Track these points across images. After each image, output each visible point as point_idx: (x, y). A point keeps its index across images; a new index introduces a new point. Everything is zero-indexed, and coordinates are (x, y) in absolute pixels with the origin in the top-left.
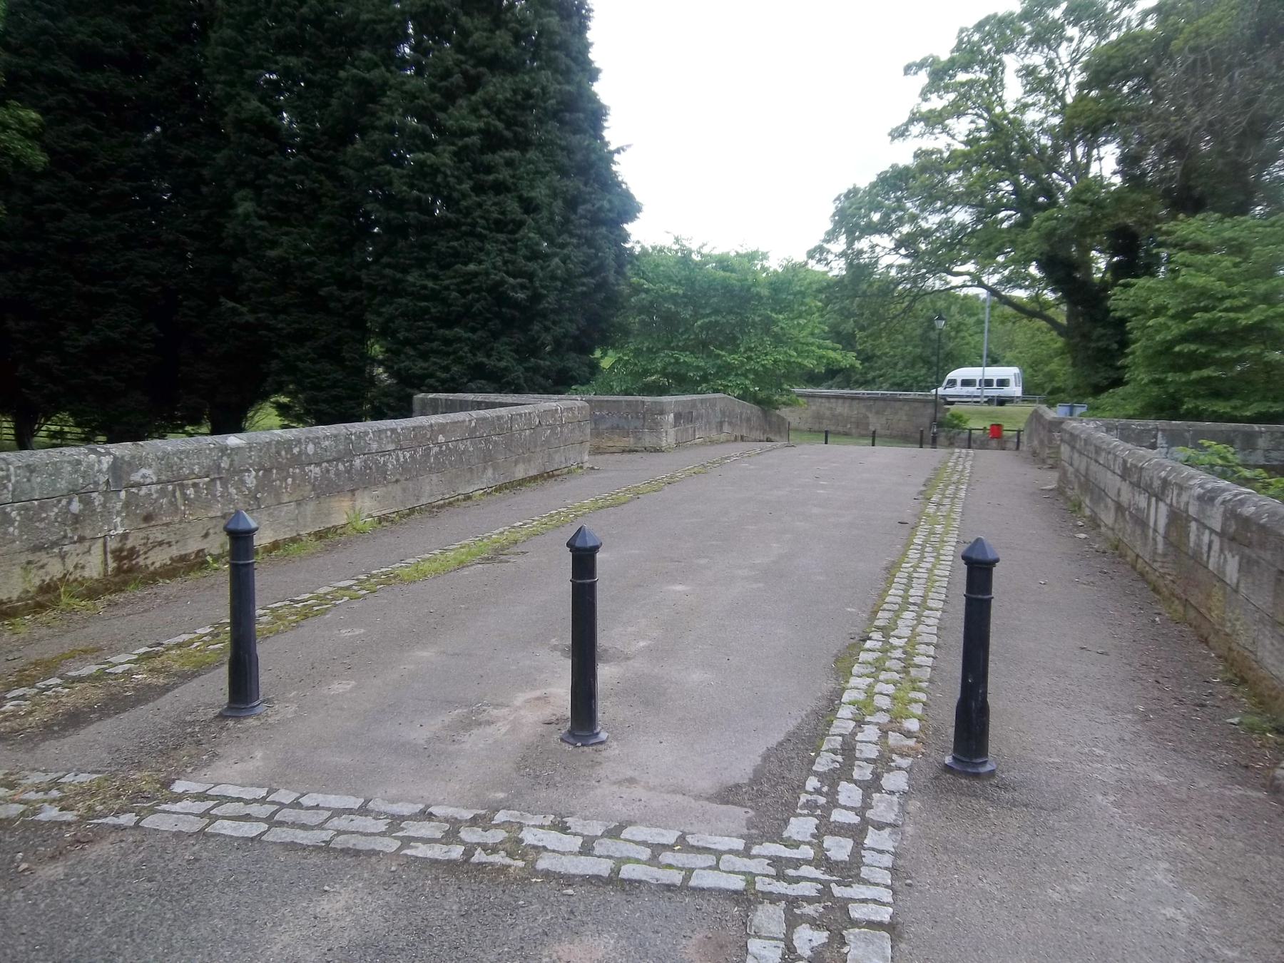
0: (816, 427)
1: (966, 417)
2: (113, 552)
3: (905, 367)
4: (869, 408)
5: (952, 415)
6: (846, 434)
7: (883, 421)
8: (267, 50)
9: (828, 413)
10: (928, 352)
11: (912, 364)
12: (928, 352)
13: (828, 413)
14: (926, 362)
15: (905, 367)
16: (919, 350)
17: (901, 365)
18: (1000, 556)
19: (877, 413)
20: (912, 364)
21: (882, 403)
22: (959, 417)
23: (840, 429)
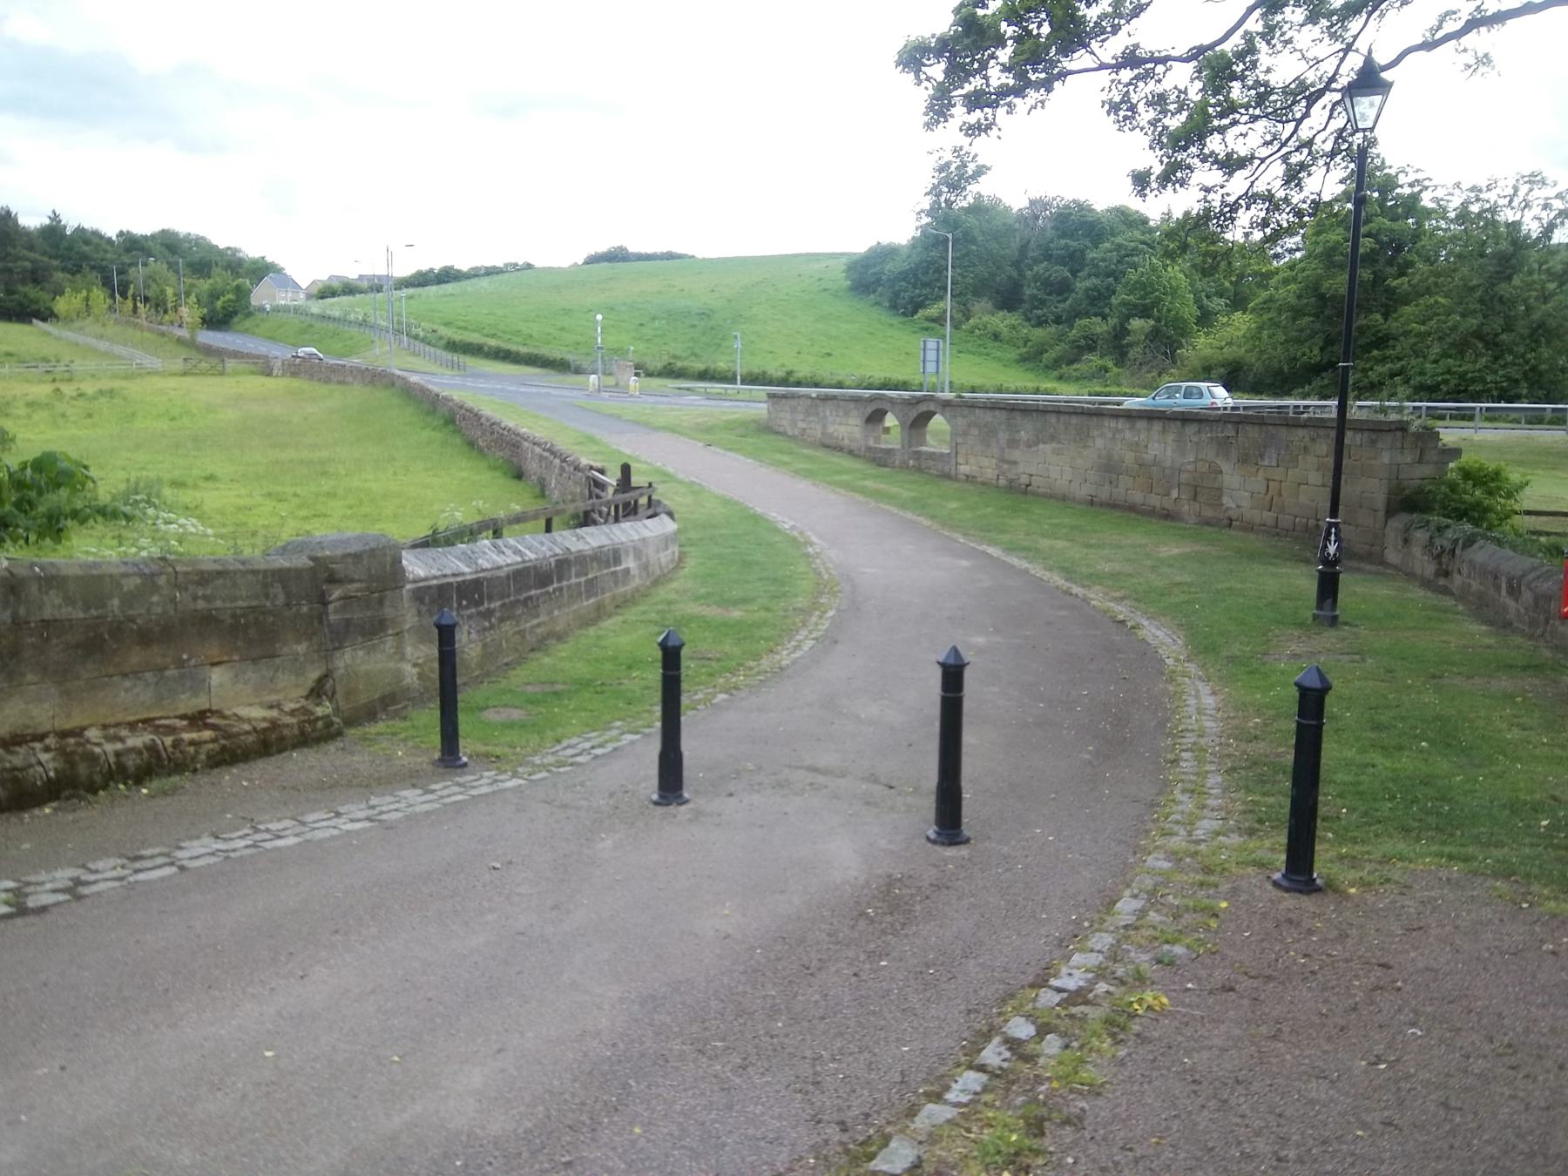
0: (1104, 494)
1: (1514, 476)
2: (1246, 32)
3: (1445, 355)
4: (1223, 445)
5: (1467, 474)
6: (1168, 516)
7: (1257, 483)
8: (250, 496)
9: (1129, 457)
10: (1497, 324)
11: (1461, 348)
12: (1497, 324)
13: (1129, 457)
14: (1492, 343)
15: (1445, 355)
16: (1473, 322)
17: (1436, 350)
18: (685, 638)
19: (1244, 460)
20: (1461, 348)
21: (1253, 432)
22: (1488, 480)
23: (1155, 501)
